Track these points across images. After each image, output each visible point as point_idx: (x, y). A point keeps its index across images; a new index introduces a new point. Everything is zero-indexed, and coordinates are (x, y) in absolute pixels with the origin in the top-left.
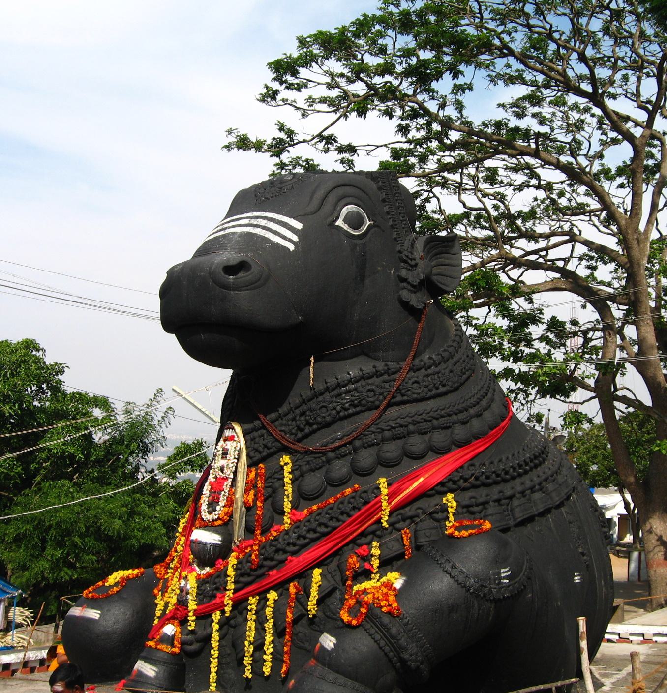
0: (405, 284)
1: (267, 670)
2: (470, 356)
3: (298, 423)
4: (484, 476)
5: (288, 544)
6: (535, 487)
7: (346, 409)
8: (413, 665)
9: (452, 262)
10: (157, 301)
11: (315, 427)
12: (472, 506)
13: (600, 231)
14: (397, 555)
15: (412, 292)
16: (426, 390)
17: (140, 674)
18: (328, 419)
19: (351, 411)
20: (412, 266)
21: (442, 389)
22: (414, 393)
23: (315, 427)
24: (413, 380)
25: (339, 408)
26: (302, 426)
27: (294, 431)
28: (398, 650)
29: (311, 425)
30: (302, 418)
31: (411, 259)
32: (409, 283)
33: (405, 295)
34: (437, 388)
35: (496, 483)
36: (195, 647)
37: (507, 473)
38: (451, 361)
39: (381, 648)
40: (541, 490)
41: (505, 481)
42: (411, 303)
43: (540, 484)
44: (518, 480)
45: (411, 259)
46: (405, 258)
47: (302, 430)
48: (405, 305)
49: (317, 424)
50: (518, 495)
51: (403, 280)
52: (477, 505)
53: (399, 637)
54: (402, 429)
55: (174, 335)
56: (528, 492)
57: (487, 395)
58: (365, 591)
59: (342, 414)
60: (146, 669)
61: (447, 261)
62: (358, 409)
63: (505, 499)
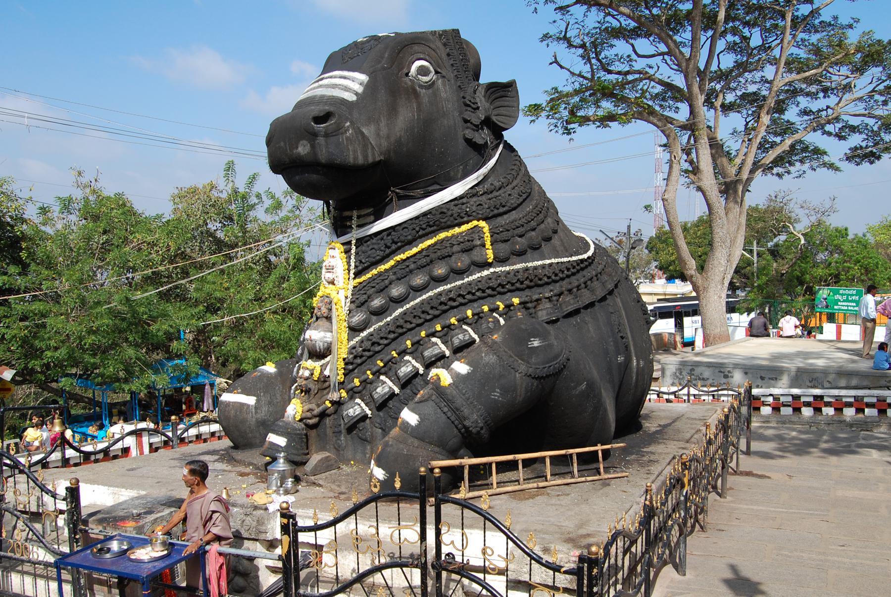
0: (469, 124)
1: (216, 427)
2: (527, 181)
3: (386, 241)
4: (537, 278)
5: (382, 338)
6: (580, 285)
7: (424, 229)
8: (474, 431)
9: (511, 104)
10: (265, 149)
11: (399, 244)
12: (527, 303)
13: (671, 68)
14: (716, 363)
15: (474, 130)
16: (488, 210)
17: (272, 444)
18: (410, 237)
19: (427, 231)
20: (475, 109)
21: (502, 210)
22: (478, 214)
23: (399, 244)
24: (478, 203)
25: (417, 229)
26: (389, 244)
27: (382, 248)
28: (462, 419)
29: (396, 243)
30: (389, 238)
31: (474, 103)
32: (471, 123)
33: (469, 134)
34: (498, 209)
35: (548, 284)
36: (314, 421)
37: (556, 275)
38: (510, 186)
39: (448, 418)
40: (586, 287)
41: (556, 282)
42: (474, 140)
43: (585, 283)
44: (567, 280)
45: (474, 103)
46: (468, 103)
47: (389, 247)
48: (469, 142)
49: (401, 242)
50: (566, 292)
51: (466, 121)
52: (531, 302)
53: (462, 409)
54: (469, 244)
55: (280, 176)
56: (575, 290)
57: (541, 212)
58: (211, 357)
59: (420, 233)
60: (278, 440)
61: (506, 104)
62: (432, 228)
63: (555, 296)
